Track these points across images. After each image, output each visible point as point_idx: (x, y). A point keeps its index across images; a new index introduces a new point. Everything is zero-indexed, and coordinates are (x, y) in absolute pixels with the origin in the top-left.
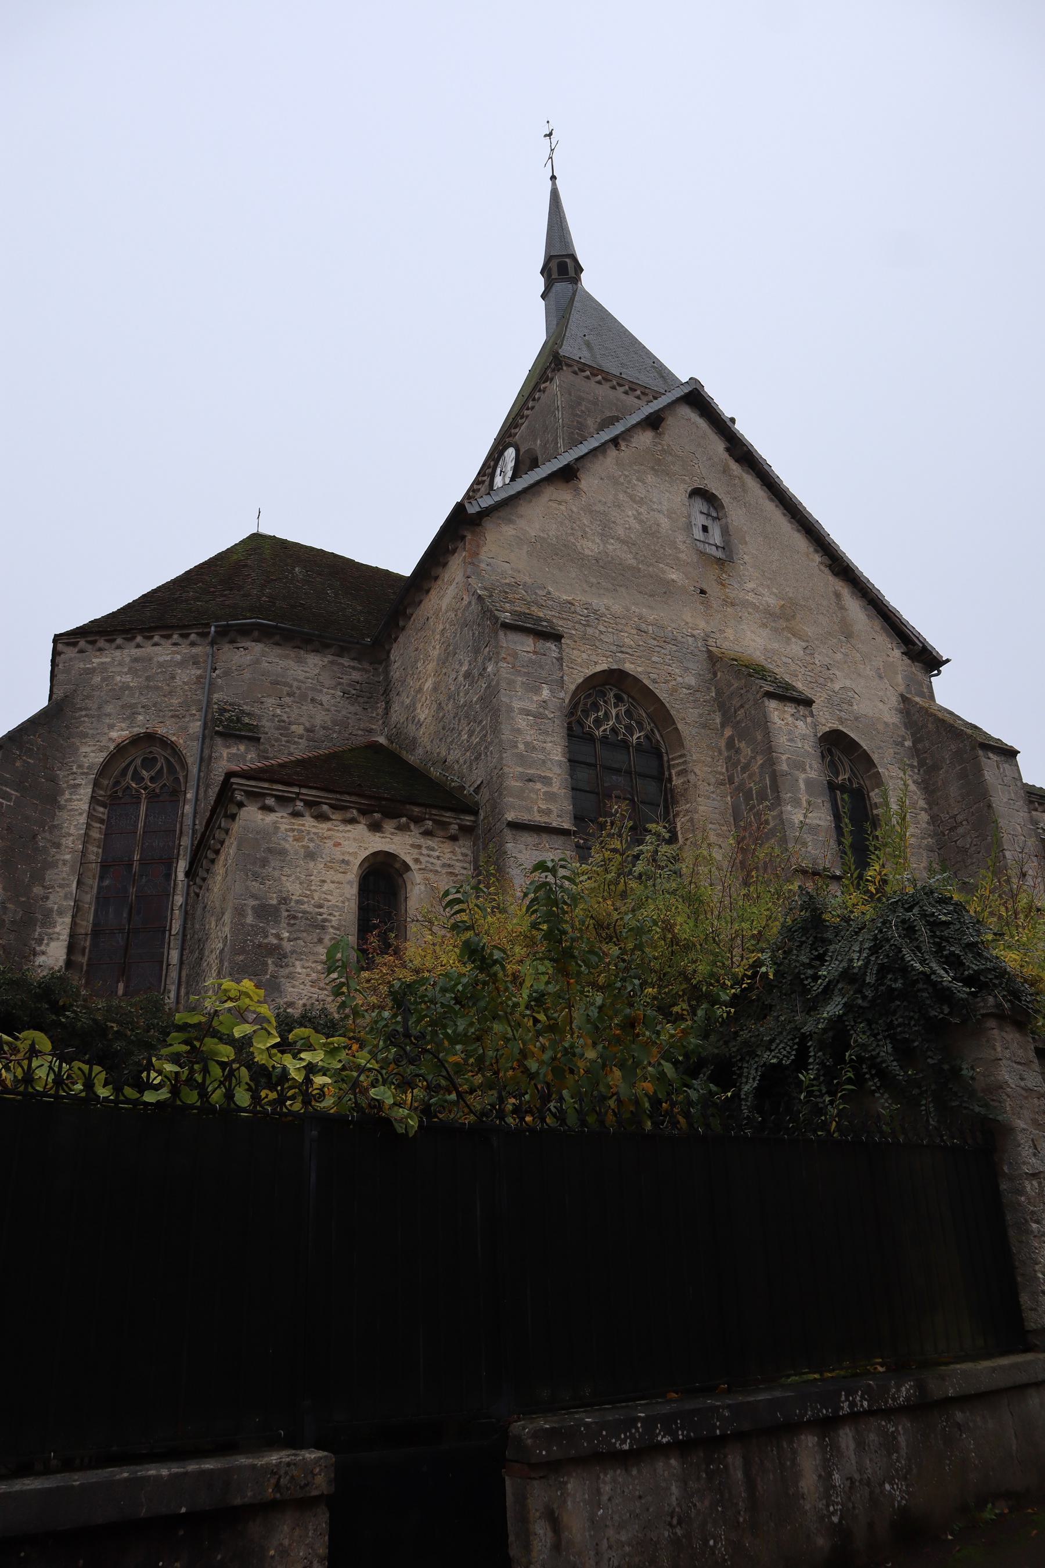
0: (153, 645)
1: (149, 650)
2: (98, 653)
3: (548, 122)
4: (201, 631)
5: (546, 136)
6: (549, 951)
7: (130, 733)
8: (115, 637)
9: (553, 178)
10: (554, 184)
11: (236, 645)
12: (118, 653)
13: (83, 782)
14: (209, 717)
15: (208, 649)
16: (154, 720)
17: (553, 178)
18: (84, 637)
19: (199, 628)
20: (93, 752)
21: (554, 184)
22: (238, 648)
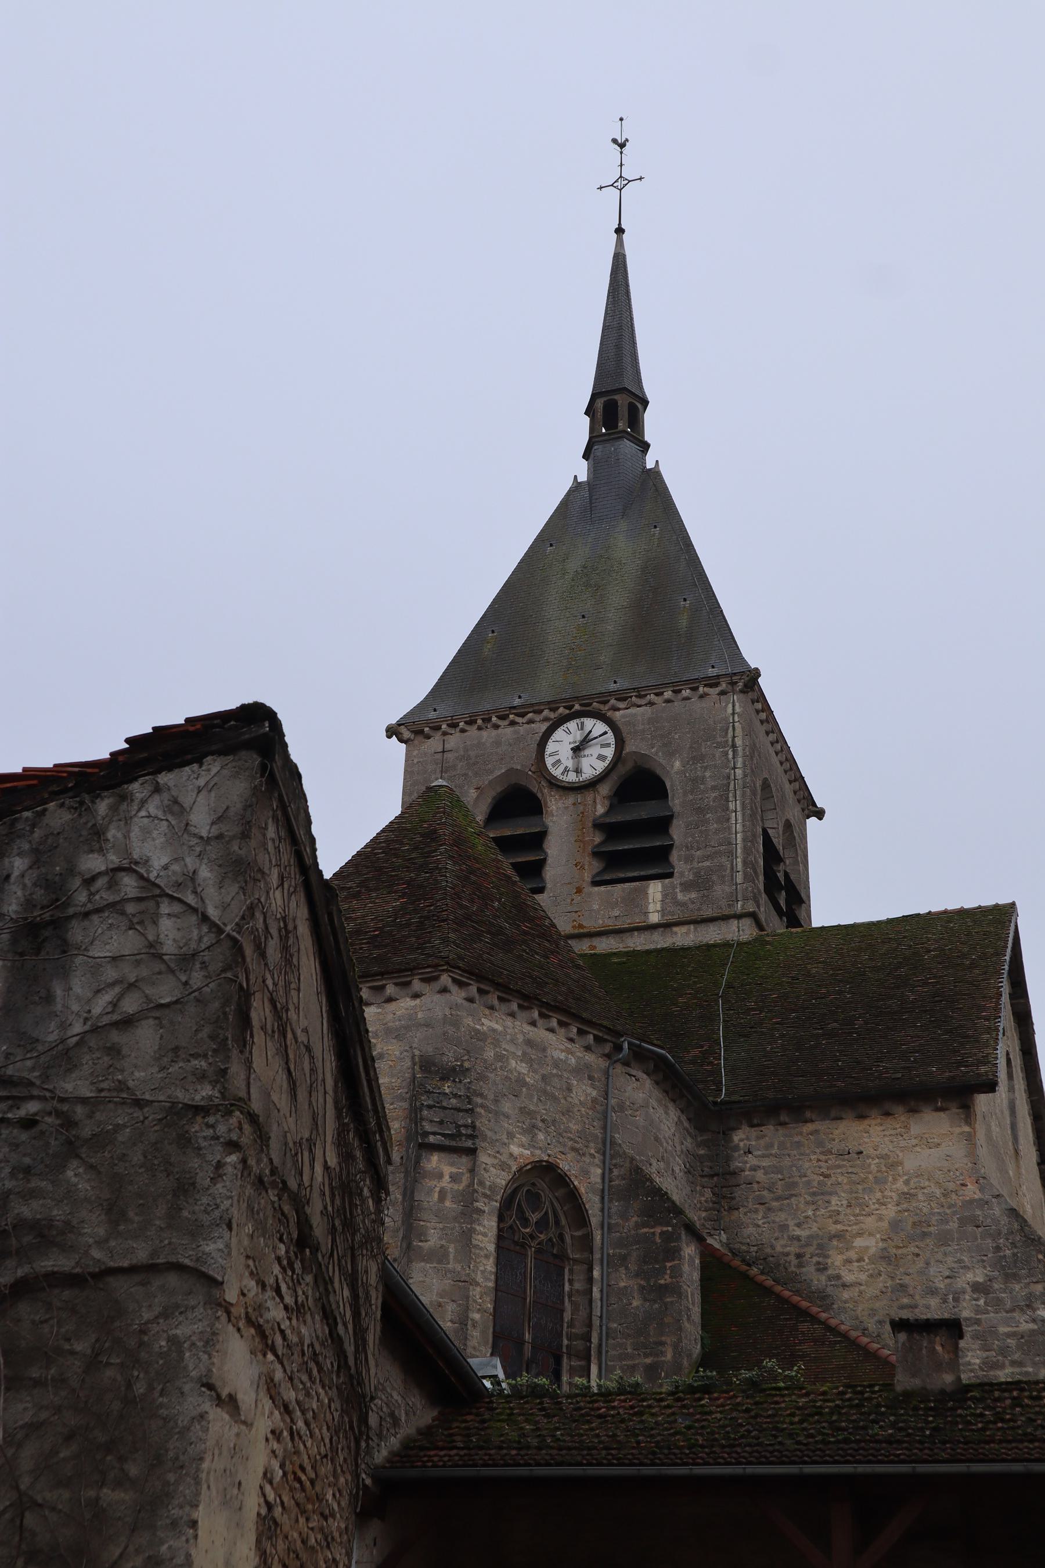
0: (547, 1029)
1: (540, 1034)
2: (487, 1012)
3: (621, 119)
4: (601, 1034)
5: (615, 141)
6: (218, 1225)
7: (533, 1154)
8: (510, 998)
9: (620, 231)
10: (620, 243)
11: (629, 1070)
12: (509, 1021)
13: (486, 1209)
14: (296, 974)
15: (603, 1063)
16: (555, 1146)
17: (620, 231)
18: (478, 981)
19: (601, 1031)
20: (494, 1166)
21: (620, 243)
22: (630, 1075)
